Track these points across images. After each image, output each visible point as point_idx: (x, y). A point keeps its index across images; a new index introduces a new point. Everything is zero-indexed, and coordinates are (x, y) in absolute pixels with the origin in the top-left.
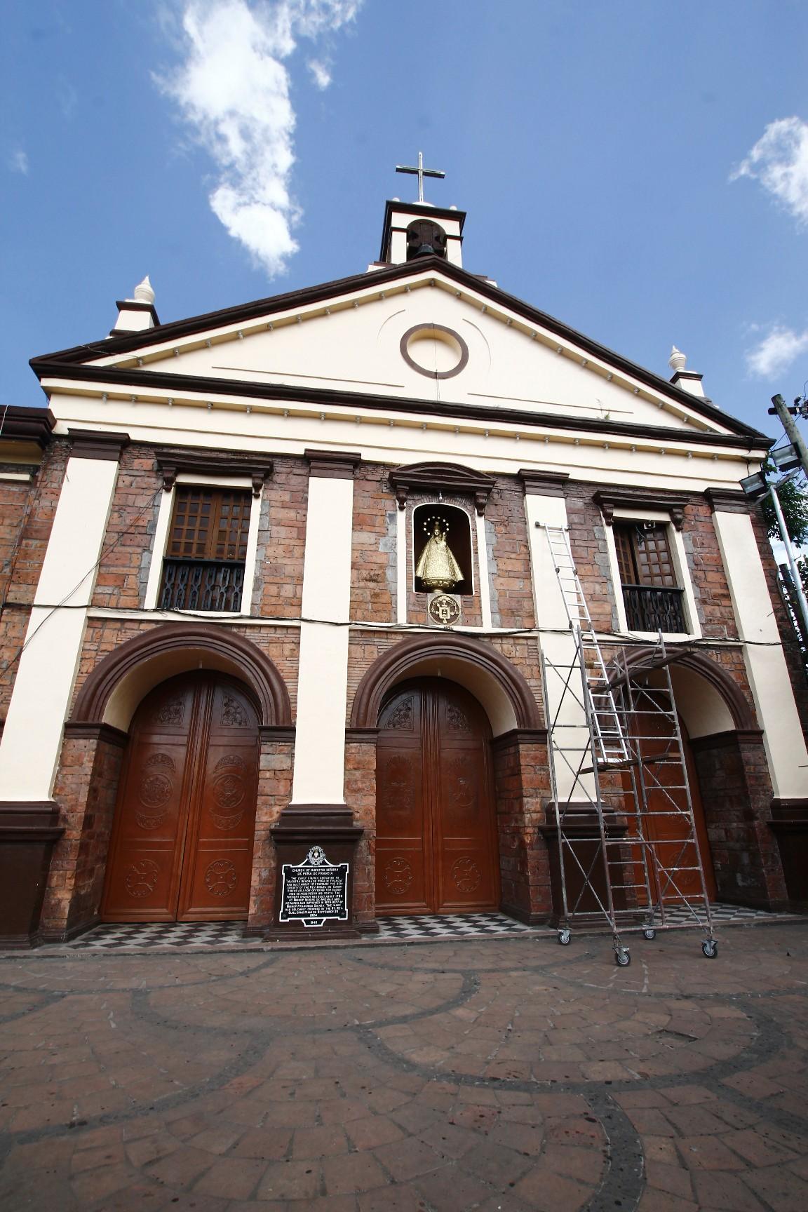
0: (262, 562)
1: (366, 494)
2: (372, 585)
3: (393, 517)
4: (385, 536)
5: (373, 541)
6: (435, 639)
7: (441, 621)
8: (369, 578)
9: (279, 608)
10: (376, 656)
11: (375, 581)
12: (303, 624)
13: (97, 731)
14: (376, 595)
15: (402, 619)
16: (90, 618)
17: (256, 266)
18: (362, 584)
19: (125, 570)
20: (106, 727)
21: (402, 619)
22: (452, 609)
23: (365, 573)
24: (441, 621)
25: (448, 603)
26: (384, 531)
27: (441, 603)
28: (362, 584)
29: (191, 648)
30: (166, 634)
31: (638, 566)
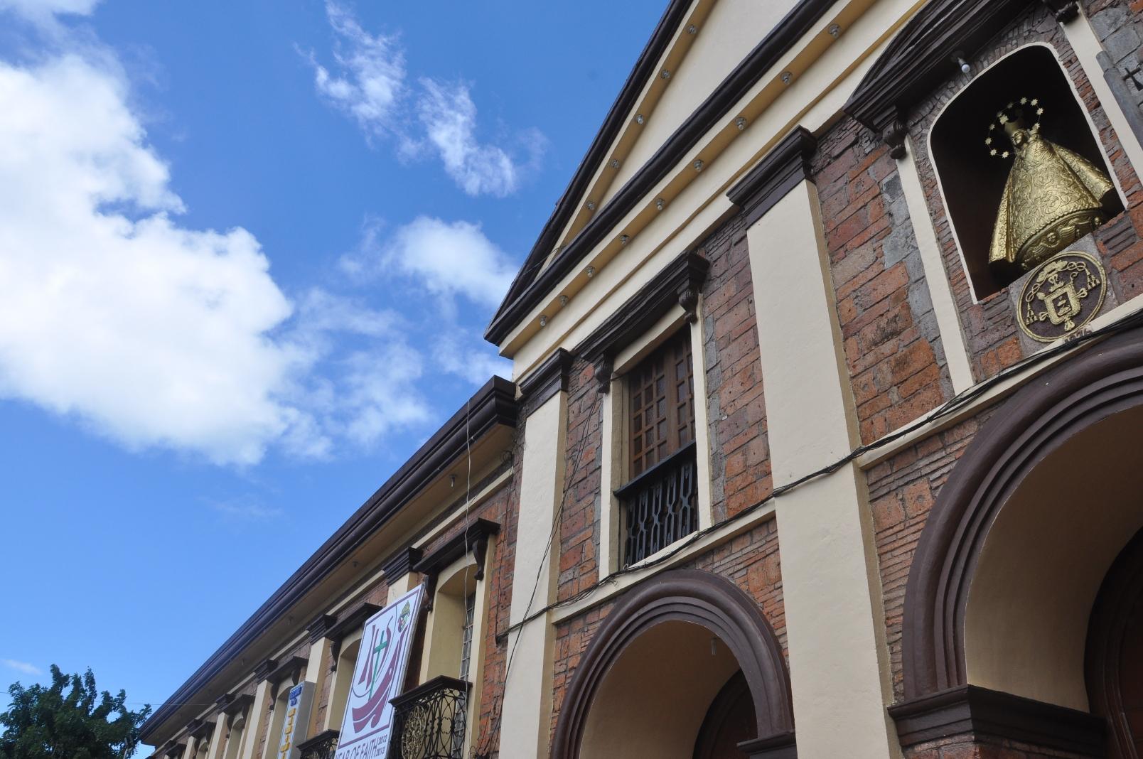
0: (718, 422)
1: (840, 183)
2: (887, 347)
3: (894, 186)
4: (888, 231)
5: (870, 257)
6: (1049, 387)
7: (1059, 329)
8: (878, 336)
9: (749, 490)
10: (928, 502)
11: (895, 333)
12: (778, 505)
13: (965, 712)
14: (902, 363)
15: (962, 380)
16: (558, 625)
17: (250, 455)
18: (870, 358)
19: (581, 536)
20: (976, 697)
21: (962, 380)
22: (1079, 280)
23: (870, 333)
24: (1059, 329)
25: (1064, 275)
26: (885, 222)
27: (1046, 286)
28: (870, 358)
29: (659, 621)
30: (620, 613)
31: (501, 495)
